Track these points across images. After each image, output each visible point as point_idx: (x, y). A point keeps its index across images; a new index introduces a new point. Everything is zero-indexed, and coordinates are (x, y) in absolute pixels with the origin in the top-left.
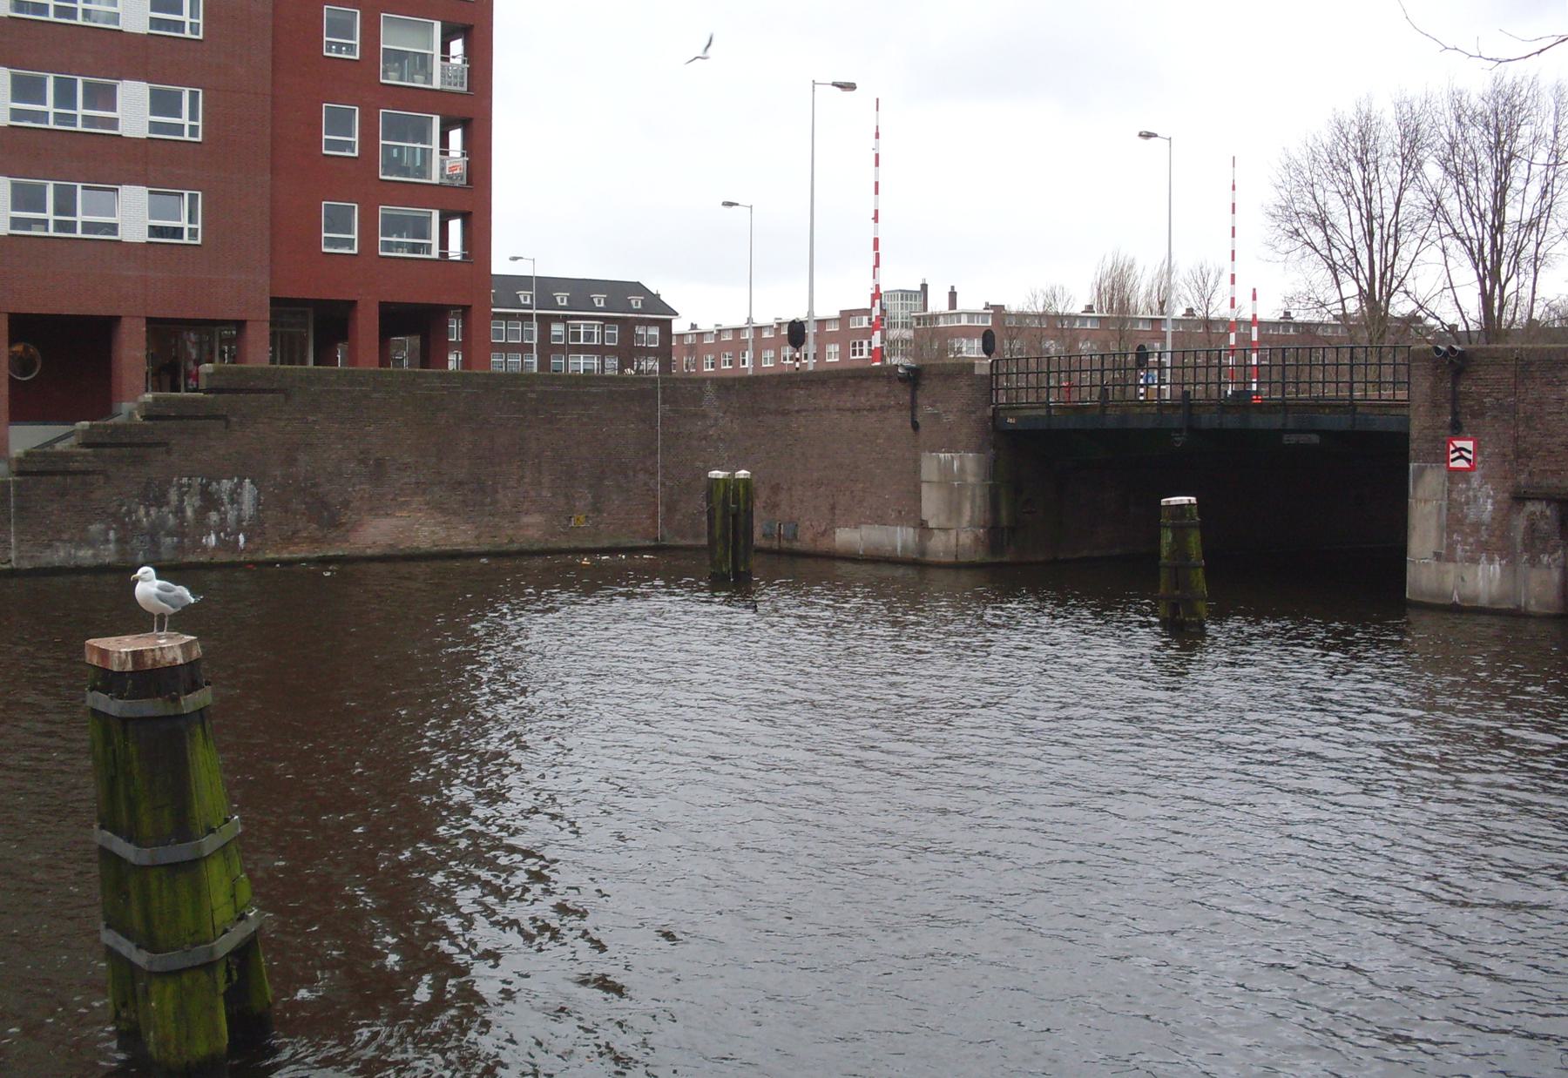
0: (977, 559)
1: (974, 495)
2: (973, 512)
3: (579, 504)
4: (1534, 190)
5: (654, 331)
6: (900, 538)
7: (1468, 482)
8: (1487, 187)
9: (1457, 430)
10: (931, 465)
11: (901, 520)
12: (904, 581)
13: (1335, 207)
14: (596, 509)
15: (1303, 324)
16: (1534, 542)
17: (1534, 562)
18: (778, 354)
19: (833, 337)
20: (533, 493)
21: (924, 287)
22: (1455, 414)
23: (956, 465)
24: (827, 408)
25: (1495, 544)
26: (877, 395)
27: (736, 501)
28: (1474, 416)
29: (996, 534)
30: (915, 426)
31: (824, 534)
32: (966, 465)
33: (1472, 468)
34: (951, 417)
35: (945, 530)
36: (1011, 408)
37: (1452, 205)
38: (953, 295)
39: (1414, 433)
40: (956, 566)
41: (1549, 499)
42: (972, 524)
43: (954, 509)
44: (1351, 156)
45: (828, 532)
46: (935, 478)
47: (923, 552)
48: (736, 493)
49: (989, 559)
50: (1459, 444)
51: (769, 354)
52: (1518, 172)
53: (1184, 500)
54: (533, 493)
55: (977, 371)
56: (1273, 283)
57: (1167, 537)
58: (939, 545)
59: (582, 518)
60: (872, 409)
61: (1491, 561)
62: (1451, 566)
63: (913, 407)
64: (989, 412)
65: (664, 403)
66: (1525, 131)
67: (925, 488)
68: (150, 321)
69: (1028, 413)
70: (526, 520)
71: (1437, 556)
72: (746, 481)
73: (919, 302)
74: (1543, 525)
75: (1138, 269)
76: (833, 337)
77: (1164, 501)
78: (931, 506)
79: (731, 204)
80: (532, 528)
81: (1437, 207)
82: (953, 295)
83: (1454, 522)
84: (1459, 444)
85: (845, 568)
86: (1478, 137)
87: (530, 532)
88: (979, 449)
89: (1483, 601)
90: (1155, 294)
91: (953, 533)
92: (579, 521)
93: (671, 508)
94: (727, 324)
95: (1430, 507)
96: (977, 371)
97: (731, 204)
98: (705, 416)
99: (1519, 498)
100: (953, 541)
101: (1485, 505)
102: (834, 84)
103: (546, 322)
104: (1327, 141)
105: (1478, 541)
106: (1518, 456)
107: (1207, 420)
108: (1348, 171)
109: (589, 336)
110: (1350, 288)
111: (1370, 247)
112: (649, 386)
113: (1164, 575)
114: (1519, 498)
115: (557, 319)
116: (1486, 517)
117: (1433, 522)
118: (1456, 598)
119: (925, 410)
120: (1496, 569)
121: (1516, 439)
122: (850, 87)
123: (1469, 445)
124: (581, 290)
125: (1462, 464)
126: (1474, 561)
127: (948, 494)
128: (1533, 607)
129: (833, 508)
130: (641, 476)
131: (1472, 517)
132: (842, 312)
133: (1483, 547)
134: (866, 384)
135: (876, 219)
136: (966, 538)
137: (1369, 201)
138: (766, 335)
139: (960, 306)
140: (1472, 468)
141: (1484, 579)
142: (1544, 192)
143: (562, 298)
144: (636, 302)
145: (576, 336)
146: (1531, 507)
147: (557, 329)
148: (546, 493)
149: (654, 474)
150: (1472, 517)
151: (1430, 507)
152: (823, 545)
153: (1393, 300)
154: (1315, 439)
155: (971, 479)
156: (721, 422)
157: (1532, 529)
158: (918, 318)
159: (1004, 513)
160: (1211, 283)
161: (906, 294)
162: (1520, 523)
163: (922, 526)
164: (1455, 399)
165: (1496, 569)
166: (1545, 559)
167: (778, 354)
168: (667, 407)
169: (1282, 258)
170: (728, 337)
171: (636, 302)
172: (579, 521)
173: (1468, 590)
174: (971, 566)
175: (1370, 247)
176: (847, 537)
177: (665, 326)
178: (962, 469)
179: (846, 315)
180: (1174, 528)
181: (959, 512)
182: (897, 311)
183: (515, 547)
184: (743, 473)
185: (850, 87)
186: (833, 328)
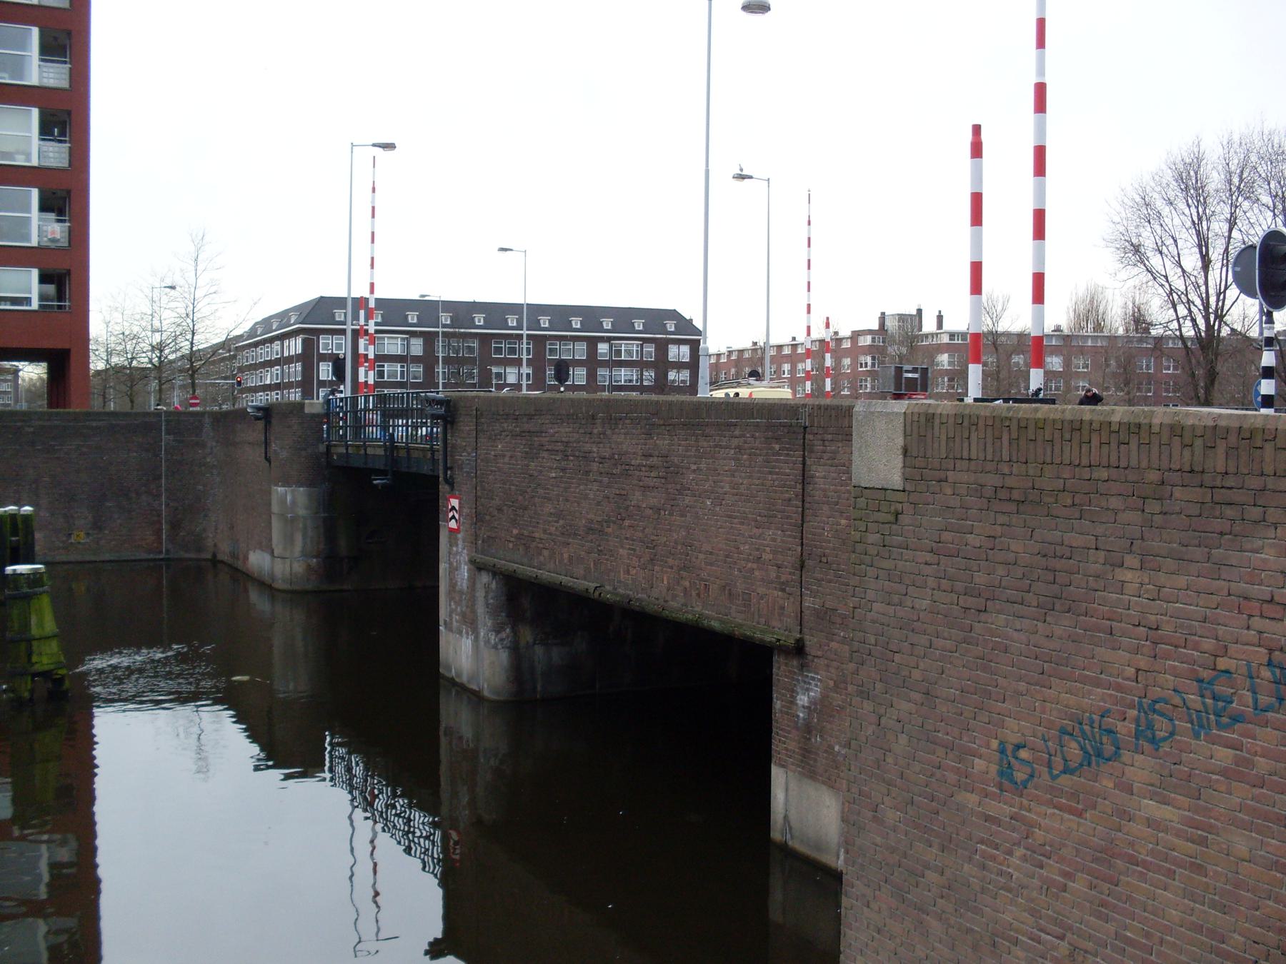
0: (310, 587)
1: (305, 528)
2: (305, 544)
5: (685, 349)
14: (97, 526)
21: (919, 311)
32: (290, 498)
38: (940, 318)
42: (304, 554)
59: (82, 534)
61: (674, 381)
64: (322, 448)
65: (168, 433)
68: (69, 350)
72: (27, 518)
75: (1109, 294)
76: (847, 353)
77: (9, 569)
82: (940, 318)
88: (310, 484)
91: (288, 561)
92: (80, 537)
100: (288, 569)
102: (374, 145)
103: (592, 343)
109: (629, 353)
112: (153, 420)
115: (602, 339)
122: (389, 146)
124: (624, 317)
130: (144, 497)
136: (299, 568)
143: (607, 324)
144: (671, 326)
145: (619, 353)
147: (603, 348)
149: (159, 496)
168: (171, 437)
171: (671, 326)
177: (695, 346)
178: (294, 502)
179: (856, 335)
184: (27, 509)
185: (389, 146)
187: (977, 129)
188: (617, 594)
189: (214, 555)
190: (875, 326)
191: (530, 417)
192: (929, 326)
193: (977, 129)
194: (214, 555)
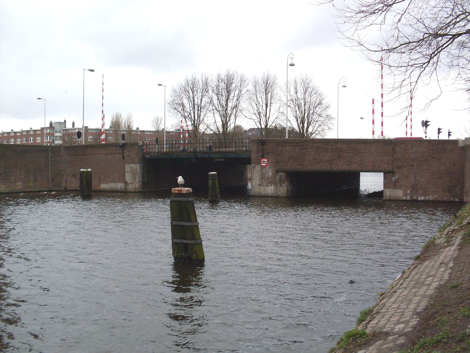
3: (31, 179)
4: (235, 99)
6: (120, 186)
7: (266, 168)
8: (224, 98)
9: (263, 157)
10: (128, 168)
11: (119, 181)
12: (123, 194)
13: (186, 102)
14: (35, 181)
15: (142, 131)
16: (281, 181)
17: (281, 186)
18: (22, 140)
19: (39, 135)
20: (19, 177)
21: (65, 121)
22: (263, 153)
23: (135, 167)
24: (98, 154)
25: (273, 182)
26: (112, 150)
27: (88, 177)
28: (267, 154)
29: (144, 184)
30: (123, 158)
31: (97, 186)
32: (137, 167)
33: (267, 165)
34: (133, 156)
35: (132, 183)
36: (148, 153)
37: (215, 101)
38: (73, 124)
39: (252, 158)
40: (135, 192)
41: (284, 172)
43: (134, 178)
44: (190, 89)
45: (99, 185)
46: (129, 171)
47: (126, 189)
48: (88, 175)
49: (143, 190)
50: (263, 160)
51: (19, 140)
52: (232, 94)
53: (215, 173)
54: (19, 177)
55: (460, 145)
56: (172, 123)
57: (210, 182)
58: (131, 187)
60: (111, 154)
61: (271, 186)
62: (262, 187)
63: (123, 153)
66: (234, 85)
67: (126, 173)
69: (152, 154)
70: (18, 184)
71: (259, 185)
73: (64, 125)
74: (283, 177)
77: (209, 173)
78: (128, 178)
79: (40, 99)
80: (19, 186)
81: (211, 102)
82: (73, 124)
83: (263, 177)
84: (263, 160)
85: (108, 194)
86: (223, 85)
87: (18, 187)
88: (140, 163)
89: (270, 195)
90: (126, 123)
92: (31, 184)
93: (53, 180)
94: (5, 131)
95: (257, 174)
96: (460, 145)
97: (40, 99)
98: (61, 156)
99: (277, 172)
100: (134, 186)
101: (270, 173)
104: (183, 84)
105: (269, 182)
106: (277, 163)
107: (199, 156)
108: (188, 92)
110: (189, 123)
111: (194, 112)
113: (210, 191)
114: (277, 172)
116: (270, 176)
117: (258, 178)
118: (264, 194)
119: (126, 154)
120: (273, 187)
121: (276, 159)
122: (92, 71)
123: (266, 160)
125: (264, 164)
126: (268, 186)
127: (133, 174)
128: (281, 195)
129: (100, 179)
130: (45, 172)
131: (267, 176)
132: (41, 128)
133: (270, 183)
134: (109, 147)
135: (103, 105)
136: (137, 185)
137: (194, 101)
138: (18, 134)
139: (76, 127)
140: (267, 165)
141: (270, 190)
142: (237, 100)
146: (281, 173)
148: (22, 176)
150: (267, 176)
151: (257, 174)
152: (97, 188)
153: (200, 126)
154: (223, 160)
155: (138, 171)
156: (66, 158)
157: (280, 178)
158: (64, 130)
159: (145, 179)
160: (159, 122)
161: (60, 123)
162: (278, 177)
163: (126, 183)
164: (263, 150)
165: (273, 187)
166: (283, 185)
167: (22, 140)
169: (172, 115)
170: (6, 135)
172: (31, 184)
173: (266, 192)
174: (139, 192)
175: (194, 112)
176: (104, 186)
178: (136, 168)
179: (43, 129)
180: (212, 179)
181: (136, 179)
182: (57, 128)
183: (15, 191)
184: (89, 170)
185: (92, 71)
186: (39, 133)
187: (373, 99)
188: (107, 200)
189: (66, 188)
190: (48, 126)
191: (302, 143)
192: (69, 126)
193: (373, 99)
194: (66, 188)
